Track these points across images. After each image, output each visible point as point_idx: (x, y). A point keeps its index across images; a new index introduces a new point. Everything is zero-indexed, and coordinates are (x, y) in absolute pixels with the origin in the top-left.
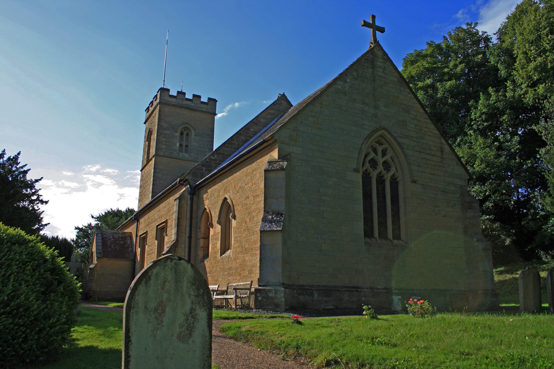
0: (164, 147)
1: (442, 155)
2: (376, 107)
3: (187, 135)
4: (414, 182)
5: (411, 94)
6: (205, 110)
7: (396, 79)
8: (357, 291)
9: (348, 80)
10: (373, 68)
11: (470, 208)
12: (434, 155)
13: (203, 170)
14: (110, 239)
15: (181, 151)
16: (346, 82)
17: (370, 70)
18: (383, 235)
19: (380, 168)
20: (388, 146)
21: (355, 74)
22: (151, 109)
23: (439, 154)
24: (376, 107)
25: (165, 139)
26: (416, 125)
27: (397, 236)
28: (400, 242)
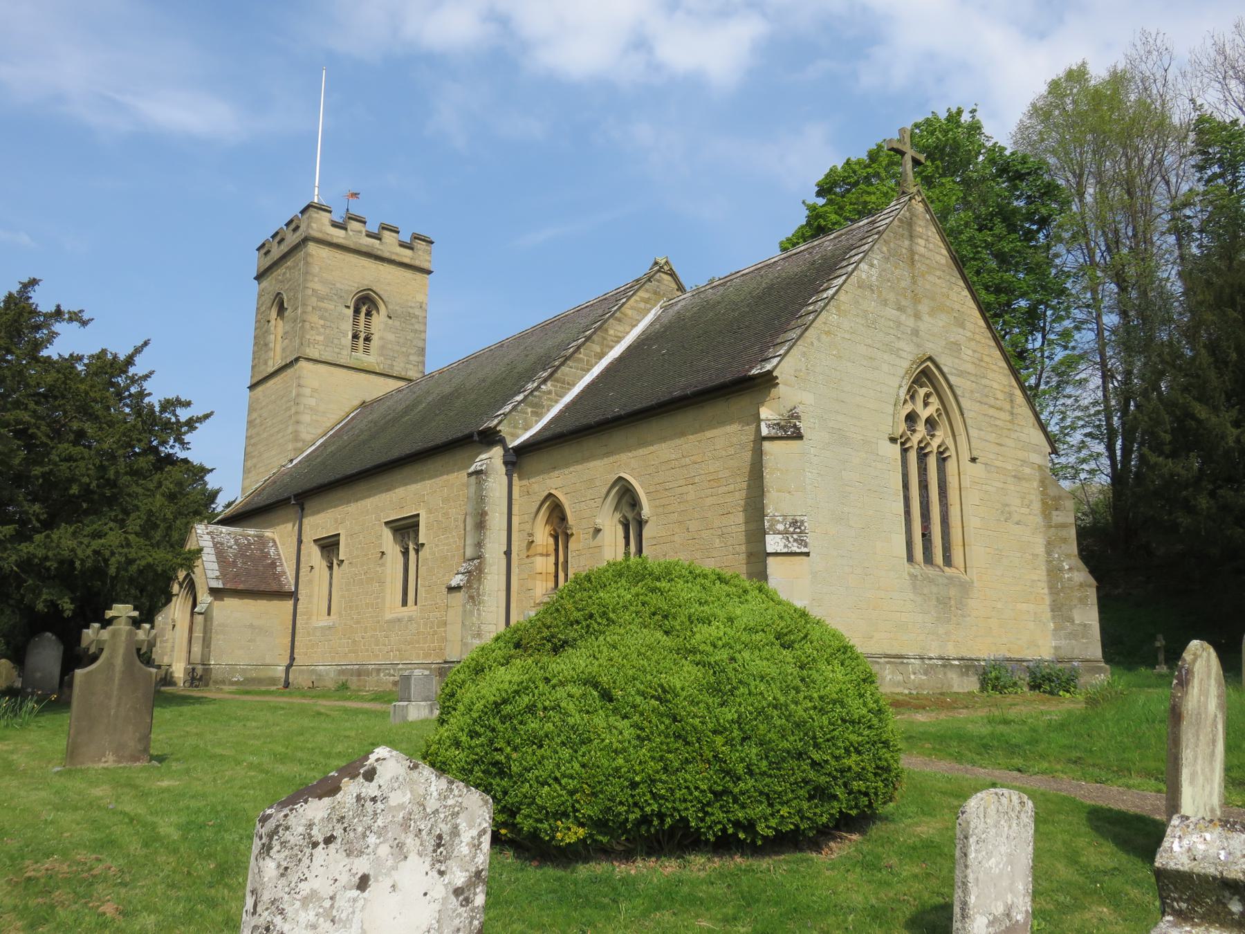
0: (321, 338)
1: (1012, 407)
2: (917, 316)
3: (368, 314)
4: (973, 460)
5: (966, 290)
6: (407, 261)
7: (943, 261)
8: (902, 663)
9: (875, 262)
10: (911, 237)
11: (1057, 509)
12: (1000, 409)
13: (527, 413)
14: (231, 547)
15: (354, 348)
16: (872, 265)
17: (907, 243)
18: (928, 558)
19: (921, 429)
20: (932, 390)
21: (885, 249)
22: (276, 252)
23: (1008, 407)
24: (917, 316)
25: (322, 322)
26: (974, 351)
27: (948, 561)
28: (953, 570)
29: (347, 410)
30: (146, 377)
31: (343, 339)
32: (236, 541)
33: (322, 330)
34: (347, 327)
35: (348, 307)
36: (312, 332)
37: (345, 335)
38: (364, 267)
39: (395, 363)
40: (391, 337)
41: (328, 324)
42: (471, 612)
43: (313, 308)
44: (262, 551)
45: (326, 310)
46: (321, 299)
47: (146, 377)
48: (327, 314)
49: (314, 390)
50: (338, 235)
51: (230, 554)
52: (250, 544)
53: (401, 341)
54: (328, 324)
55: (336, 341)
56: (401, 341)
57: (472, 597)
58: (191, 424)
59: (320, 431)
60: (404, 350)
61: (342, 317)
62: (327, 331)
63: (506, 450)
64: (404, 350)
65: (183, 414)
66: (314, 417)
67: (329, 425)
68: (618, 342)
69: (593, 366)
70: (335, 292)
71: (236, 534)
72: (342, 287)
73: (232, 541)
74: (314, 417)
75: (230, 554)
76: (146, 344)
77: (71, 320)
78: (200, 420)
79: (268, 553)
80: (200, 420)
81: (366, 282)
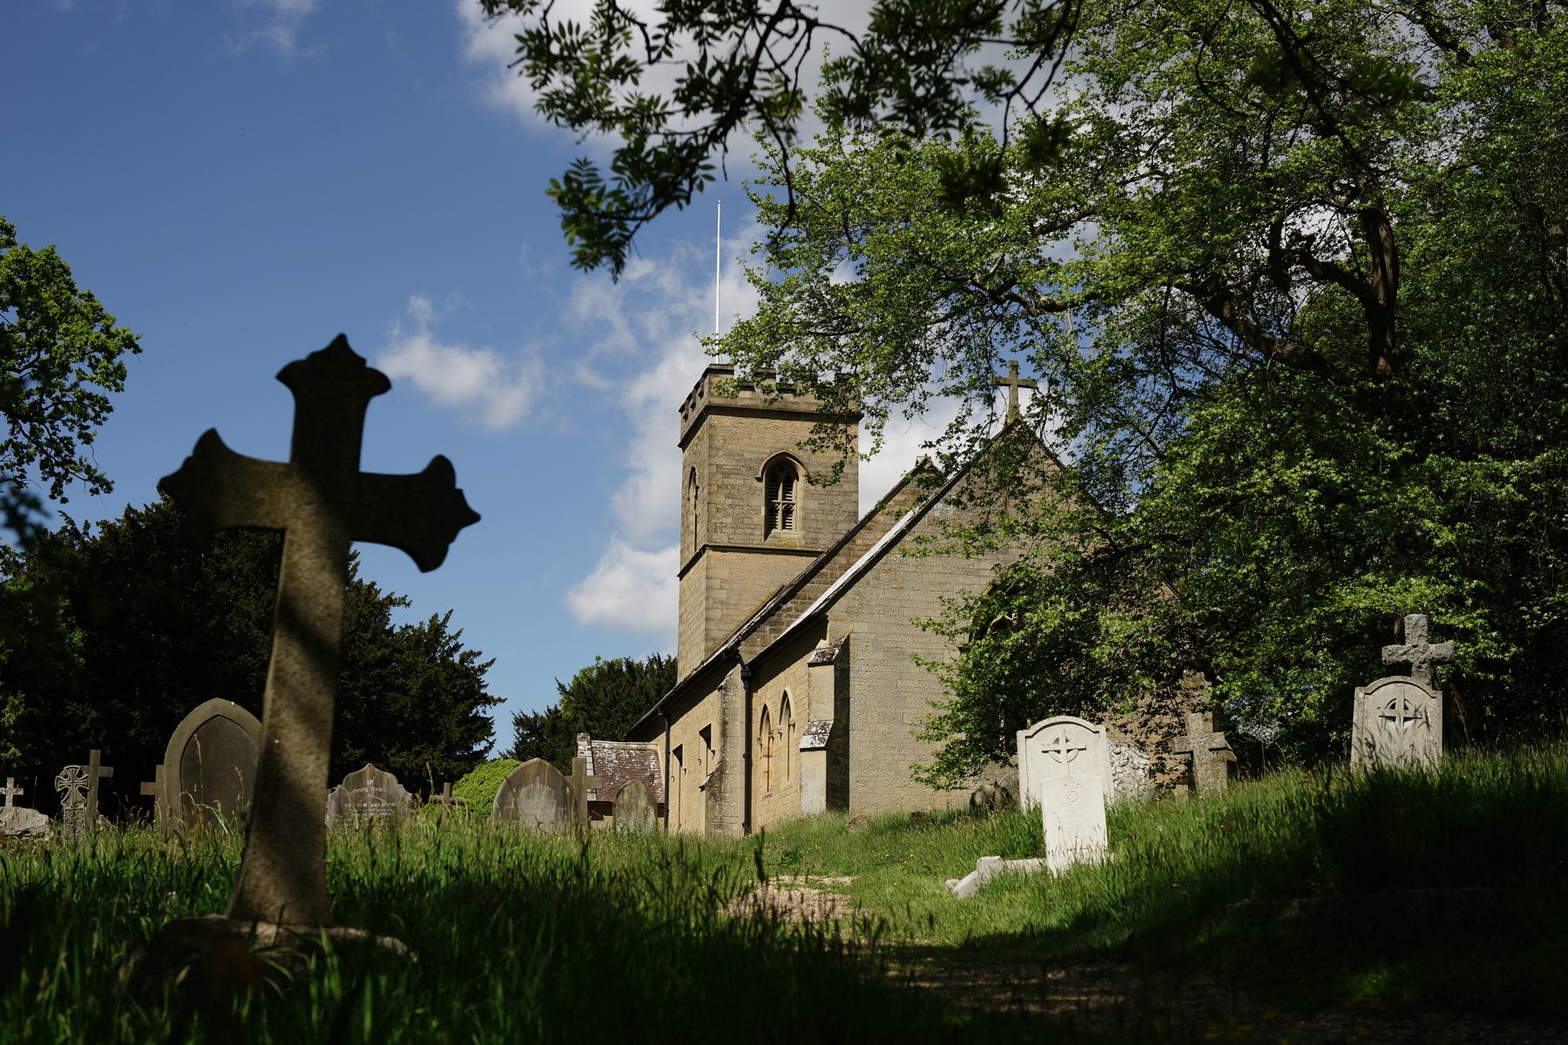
0: (729, 520)
25: (729, 501)
29: (764, 598)
30: (458, 635)
31: (755, 517)
32: (618, 755)
33: (730, 511)
34: (760, 502)
35: (759, 480)
36: (719, 515)
37: (757, 512)
38: (777, 428)
39: (819, 536)
40: (814, 505)
41: (737, 502)
42: (714, 808)
43: (719, 487)
44: (642, 764)
45: (733, 487)
46: (727, 475)
47: (458, 635)
48: (735, 492)
49: (723, 581)
50: (745, 398)
51: (610, 768)
52: (631, 757)
53: (827, 508)
54: (737, 502)
55: (746, 521)
56: (827, 508)
57: (713, 794)
58: (482, 670)
59: (733, 627)
60: (831, 518)
61: (752, 491)
62: (737, 511)
63: (743, 666)
64: (831, 518)
65: (478, 662)
66: (725, 611)
67: (743, 618)
68: (867, 550)
69: (837, 578)
70: (742, 463)
71: (618, 749)
72: (752, 456)
73: (614, 756)
74: (725, 611)
75: (610, 768)
76: (451, 612)
77: (399, 604)
78: (488, 665)
79: (649, 766)
80: (488, 665)
81: (779, 445)
